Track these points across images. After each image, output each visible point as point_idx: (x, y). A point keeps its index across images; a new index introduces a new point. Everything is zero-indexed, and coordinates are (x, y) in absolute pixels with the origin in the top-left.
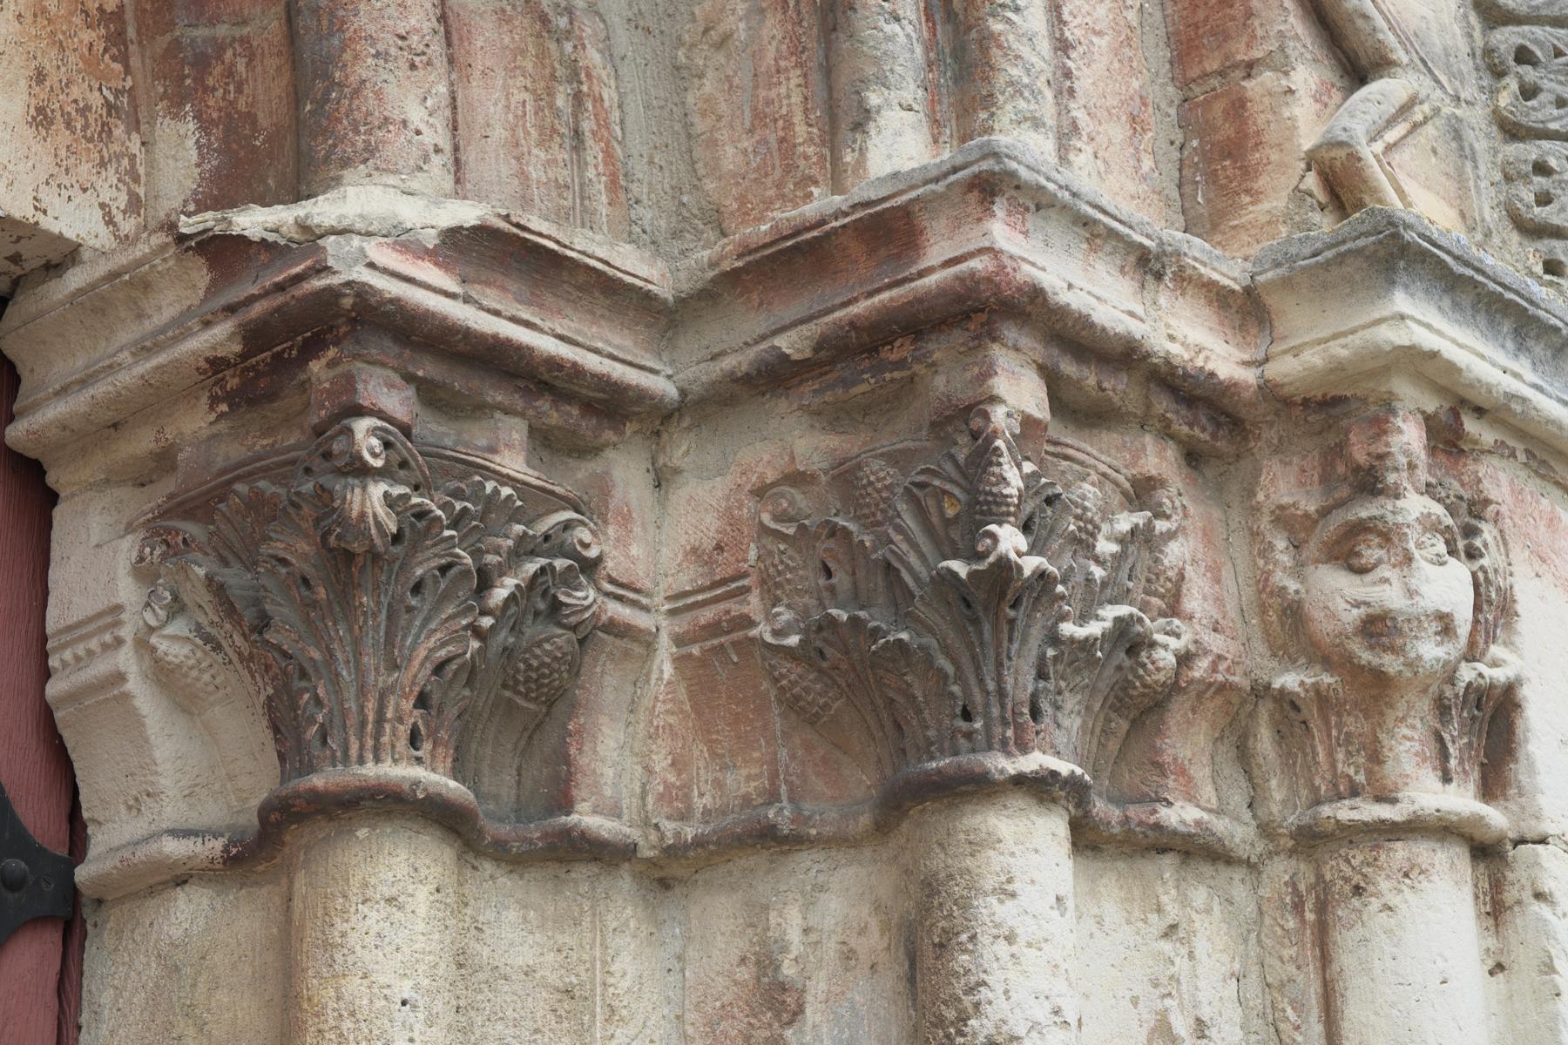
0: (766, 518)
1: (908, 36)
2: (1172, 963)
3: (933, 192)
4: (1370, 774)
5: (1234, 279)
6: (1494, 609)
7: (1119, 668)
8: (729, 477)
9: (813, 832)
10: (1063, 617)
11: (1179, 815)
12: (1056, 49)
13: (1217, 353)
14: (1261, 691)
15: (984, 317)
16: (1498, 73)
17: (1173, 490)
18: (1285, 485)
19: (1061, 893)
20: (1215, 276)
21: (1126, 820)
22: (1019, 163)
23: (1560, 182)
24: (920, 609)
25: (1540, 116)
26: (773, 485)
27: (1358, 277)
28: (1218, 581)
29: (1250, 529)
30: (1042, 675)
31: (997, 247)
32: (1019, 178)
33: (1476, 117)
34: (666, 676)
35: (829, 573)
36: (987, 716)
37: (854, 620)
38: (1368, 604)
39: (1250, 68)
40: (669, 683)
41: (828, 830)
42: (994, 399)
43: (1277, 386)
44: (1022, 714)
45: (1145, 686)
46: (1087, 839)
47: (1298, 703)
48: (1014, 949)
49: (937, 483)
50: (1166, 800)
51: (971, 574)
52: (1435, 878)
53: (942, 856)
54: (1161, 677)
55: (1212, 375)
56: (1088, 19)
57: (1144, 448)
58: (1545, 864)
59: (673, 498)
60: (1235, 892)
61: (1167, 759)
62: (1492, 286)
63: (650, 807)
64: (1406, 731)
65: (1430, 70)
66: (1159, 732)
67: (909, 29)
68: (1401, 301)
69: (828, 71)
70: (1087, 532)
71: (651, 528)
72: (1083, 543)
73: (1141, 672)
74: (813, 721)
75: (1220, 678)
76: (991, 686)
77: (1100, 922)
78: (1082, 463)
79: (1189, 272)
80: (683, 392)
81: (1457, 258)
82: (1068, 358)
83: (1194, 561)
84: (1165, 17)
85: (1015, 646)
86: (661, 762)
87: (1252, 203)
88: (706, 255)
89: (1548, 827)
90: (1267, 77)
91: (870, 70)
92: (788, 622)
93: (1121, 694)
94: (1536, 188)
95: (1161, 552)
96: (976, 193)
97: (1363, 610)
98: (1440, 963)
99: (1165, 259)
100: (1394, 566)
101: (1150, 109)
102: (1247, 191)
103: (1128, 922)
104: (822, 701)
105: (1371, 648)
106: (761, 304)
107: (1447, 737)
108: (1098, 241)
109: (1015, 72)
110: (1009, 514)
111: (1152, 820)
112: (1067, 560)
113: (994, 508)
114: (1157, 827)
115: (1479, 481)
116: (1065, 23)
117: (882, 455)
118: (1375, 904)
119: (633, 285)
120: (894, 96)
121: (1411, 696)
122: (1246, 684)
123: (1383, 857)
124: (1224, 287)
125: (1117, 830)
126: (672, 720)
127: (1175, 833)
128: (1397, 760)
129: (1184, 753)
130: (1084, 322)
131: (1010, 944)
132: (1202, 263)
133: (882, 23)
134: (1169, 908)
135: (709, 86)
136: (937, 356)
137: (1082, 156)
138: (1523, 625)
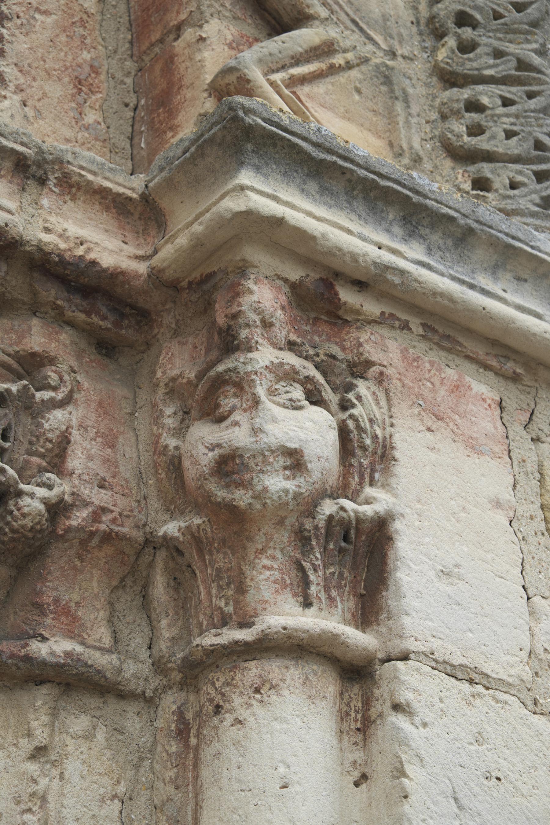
2: (35, 782)
4: (237, 603)
5: (133, 189)
6: (363, 455)
11: (54, 647)
13: (109, 248)
14: (151, 543)
16: (439, 35)
17: (64, 367)
18: (178, 361)
20: (107, 184)
23: (492, 116)
25: (475, 65)
27: (218, 166)
28: (112, 446)
33: (419, 69)
38: (219, 446)
45: (13, 531)
47: (181, 547)
50: (41, 635)
52: (286, 692)
54: (28, 522)
55: (94, 263)
57: (30, 328)
58: (402, 678)
60: (127, 724)
61: (46, 599)
62: (362, 173)
64: (266, 562)
65: (361, 30)
66: (42, 578)
68: (246, 177)
73: (9, 518)
75: (103, 527)
79: (75, 178)
81: (317, 145)
83: (82, 426)
87: (173, 137)
89: (412, 645)
90: (189, 34)
94: (469, 122)
95: (43, 417)
97: (217, 451)
98: (282, 770)
99: (46, 166)
100: (245, 411)
102: (171, 129)
105: (227, 486)
107: (307, 565)
111: (23, 652)
114: (27, 658)
115: (360, 345)
118: (229, 718)
121: (268, 528)
123: (238, 676)
124: (119, 195)
127: (44, 664)
128: (258, 588)
132: (90, 171)
138: (399, 469)
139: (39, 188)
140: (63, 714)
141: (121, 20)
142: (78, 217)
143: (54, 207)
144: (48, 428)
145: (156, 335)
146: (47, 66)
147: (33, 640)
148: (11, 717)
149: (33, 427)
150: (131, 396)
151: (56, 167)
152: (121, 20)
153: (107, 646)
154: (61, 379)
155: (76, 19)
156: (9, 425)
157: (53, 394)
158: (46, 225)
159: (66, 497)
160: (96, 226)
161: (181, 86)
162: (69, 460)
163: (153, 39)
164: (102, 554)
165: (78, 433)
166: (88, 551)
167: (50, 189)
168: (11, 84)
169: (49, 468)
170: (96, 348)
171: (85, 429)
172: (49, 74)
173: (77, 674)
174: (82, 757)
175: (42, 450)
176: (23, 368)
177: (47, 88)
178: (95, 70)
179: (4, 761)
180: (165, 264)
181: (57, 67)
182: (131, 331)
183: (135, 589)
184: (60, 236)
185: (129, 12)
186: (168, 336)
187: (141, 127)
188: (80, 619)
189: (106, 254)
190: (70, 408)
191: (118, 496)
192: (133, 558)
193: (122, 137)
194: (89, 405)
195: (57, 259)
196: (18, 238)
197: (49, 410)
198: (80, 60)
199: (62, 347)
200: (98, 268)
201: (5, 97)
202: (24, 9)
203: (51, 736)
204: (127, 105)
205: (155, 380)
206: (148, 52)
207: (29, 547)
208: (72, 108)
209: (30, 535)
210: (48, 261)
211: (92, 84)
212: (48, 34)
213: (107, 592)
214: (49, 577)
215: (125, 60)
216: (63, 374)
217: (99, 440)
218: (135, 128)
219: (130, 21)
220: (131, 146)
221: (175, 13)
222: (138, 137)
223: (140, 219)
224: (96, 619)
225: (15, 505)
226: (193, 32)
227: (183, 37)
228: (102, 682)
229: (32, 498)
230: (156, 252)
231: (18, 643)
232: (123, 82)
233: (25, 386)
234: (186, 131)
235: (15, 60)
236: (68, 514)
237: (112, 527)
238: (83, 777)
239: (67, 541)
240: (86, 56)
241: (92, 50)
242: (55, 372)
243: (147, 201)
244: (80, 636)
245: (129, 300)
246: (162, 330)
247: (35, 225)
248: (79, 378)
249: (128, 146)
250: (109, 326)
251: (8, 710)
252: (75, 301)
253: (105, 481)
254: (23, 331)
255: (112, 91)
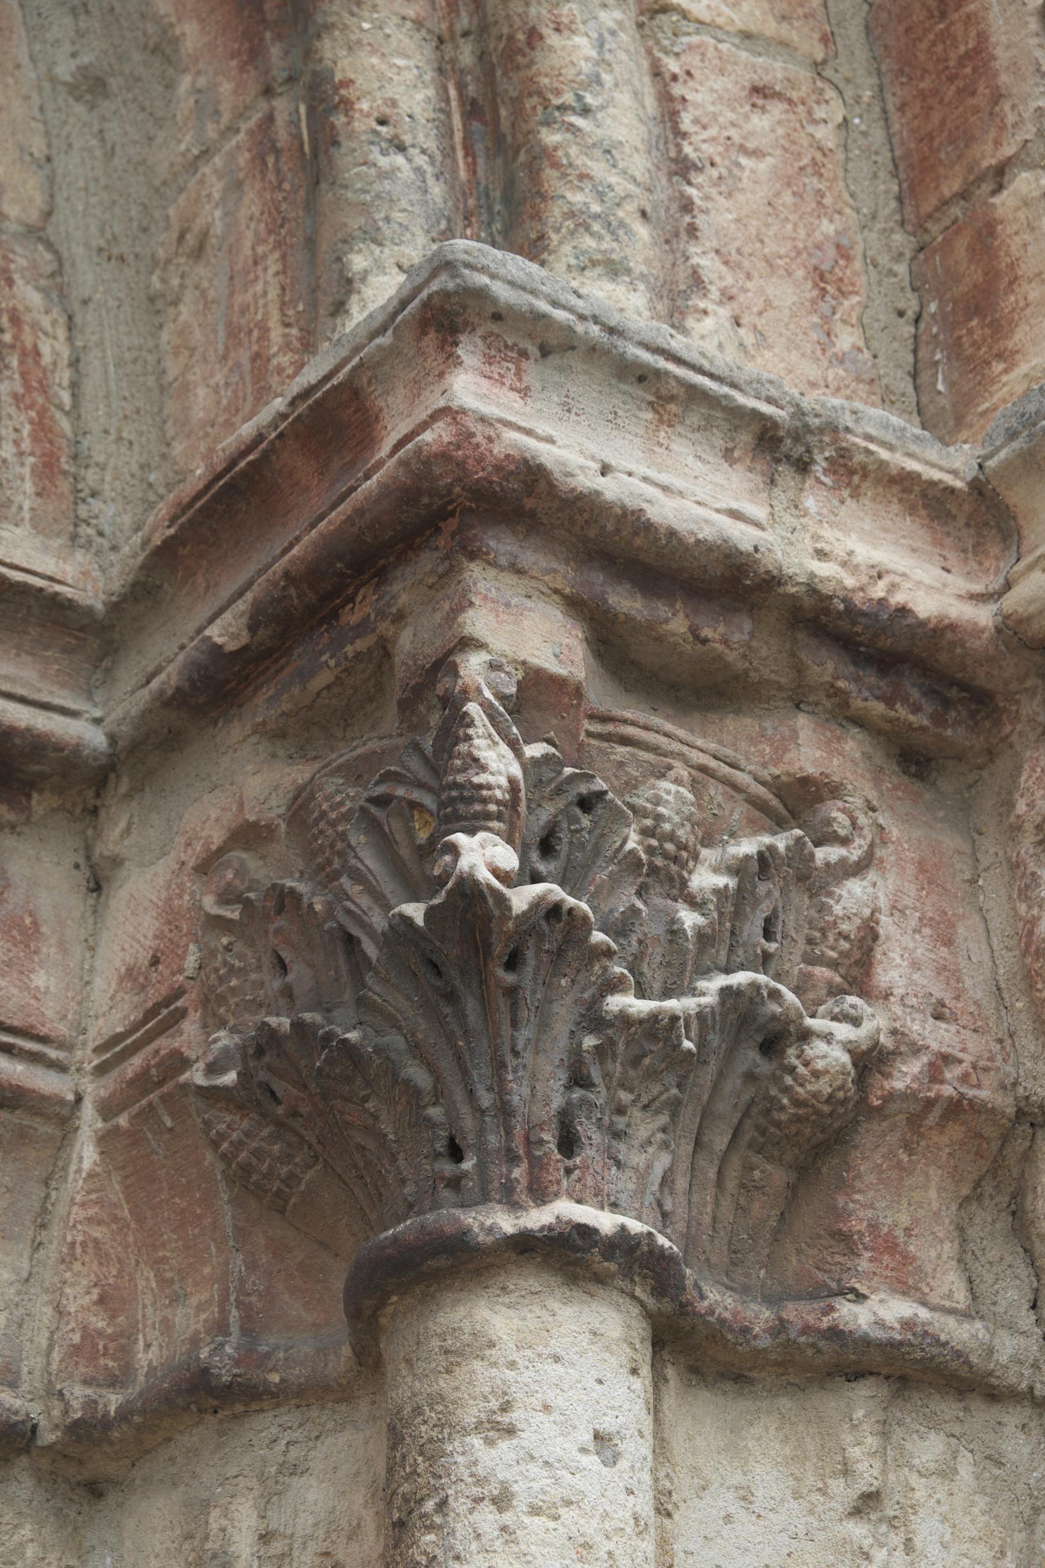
0: (209, 904)
1: (418, 170)
3: (380, 348)
5: (955, 473)
7: (750, 1077)
8: (173, 854)
9: (275, 1378)
10: (614, 986)
11: (878, 1312)
12: (671, 174)
13: (926, 584)
15: (453, 523)
17: (856, 802)
19: (608, 1424)
21: (781, 1326)
22: (493, 276)
24: (376, 989)
26: (221, 851)
28: (948, 943)
29: (1009, 860)
30: (578, 1079)
31: (455, 405)
32: (494, 300)
34: (86, 1165)
35: (283, 967)
36: (481, 1149)
37: (298, 1026)
39: (1000, 174)
40: (91, 1175)
41: (297, 1374)
42: (468, 643)
43: (1020, 621)
44: (541, 1142)
45: (797, 1103)
46: (685, 1349)
48: (508, 1518)
49: (400, 792)
50: (853, 1290)
51: (429, 914)
53: (409, 1379)
54: (823, 1086)
55: (903, 611)
56: (732, 132)
57: (795, 734)
59: (113, 903)
60: (1007, 1447)
63: (54, 1367)
66: (844, 1186)
67: (422, 161)
69: (311, 243)
70: (666, 856)
71: (77, 951)
72: (663, 871)
73: (789, 1080)
74: (279, 1204)
75: (947, 1091)
76: (486, 1100)
77: (746, 1497)
78: (654, 749)
79: (859, 458)
80: (113, 739)
82: (624, 589)
83: (895, 908)
84: (890, 137)
85: (525, 1034)
86: (79, 1298)
87: (1006, 371)
88: (127, 520)
91: (356, 223)
92: (226, 1050)
93: (762, 1121)
95: (830, 894)
96: (432, 335)
99: (809, 438)
101: (858, 264)
102: (1000, 356)
103: (797, 1495)
104: (284, 1170)
106: (207, 588)
108: (673, 408)
109: (577, 198)
110: (488, 816)
111: (826, 1322)
112: (626, 898)
113: (461, 808)
114: (835, 1333)
116: (684, 135)
117: (339, 769)
119: (25, 585)
120: (388, 254)
122: (1006, 1104)
124: (933, 484)
125: (765, 1342)
126: (97, 1232)
127: (866, 1342)
129: (896, 1217)
130: (633, 521)
131: (501, 1510)
132: (883, 444)
133: (375, 155)
134: (862, 1467)
135: (186, 312)
136: (403, 599)
137: (709, 322)
139: (798, 478)
140: (898, 1433)
141: (879, 159)
142: (866, 527)
143: (825, 511)
144: (841, 913)
145: (1007, 736)
146: (766, 250)
147: (839, 1299)
148: (808, 1440)
149: (813, 912)
150: (967, 848)
151: (827, 439)
152: (879, 159)
153: (961, 1306)
154: (854, 824)
155: (805, 161)
156: (775, 911)
157: (843, 851)
158: (818, 546)
159: (883, 1039)
160: (896, 543)
161: (1016, 278)
162: (879, 970)
163: (947, 193)
164: (944, 1140)
165: (890, 920)
166: (921, 1135)
167: (817, 479)
168: (713, 288)
169: (846, 987)
170: (899, 764)
171: (902, 912)
172: (771, 266)
173: (923, 1358)
174: (939, 1510)
175: (833, 954)
176: (785, 806)
177: (770, 291)
178: (844, 253)
179: (803, 1520)
180: (1031, 609)
181: (783, 251)
182: (961, 731)
183: (997, 1200)
184: (844, 564)
185: (891, 143)
186: (1032, 737)
187: (933, 353)
188: (914, 1258)
189: (921, 593)
190: (872, 875)
191: (967, 1034)
192: (995, 1146)
193: (899, 373)
194: (904, 869)
195: (842, 607)
196: (775, 572)
197: (839, 880)
198: (818, 236)
199: (849, 764)
200: (910, 620)
201: (705, 312)
202: (720, 149)
203: (884, 1472)
204: (901, 314)
205: (1012, 819)
206: (938, 215)
207: (823, 1131)
208: (815, 326)
209: (826, 1109)
210: (826, 611)
211: (841, 280)
212: (763, 192)
213: (954, 1207)
214: (858, 1184)
215: (892, 230)
216: (857, 814)
217: (926, 931)
218: (920, 354)
219: (893, 160)
220: (916, 388)
221: (990, 143)
222: (930, 372)
223: (967, 525)
224: (939, 1257)
225: (798, 1057)
226: (1032, 179)
227: (1011, 188)
228: (964, 1372)
229: (829, 1043)
230: (1008, 586)
231: (815, 1306)
232: (892, 273)
233: (799, 840)
234: (1034, 362)
235: (715, 244)
236: (887, 1069)
237: (962, 1090)
238: (945, 1546)
239: (886, 1118)
240: (828, 227)
241: (836, 216)
242: (843, 811)
243: (980, 493)
244: (918, 1289)
245: (959, 675)
246: (1019, 727)
247: (799, 546)
248: (881, 821)
249: (910, 389)
250: (926, 722)
251: (801, 1428)
252: (867, 680)
253: (944, 1006)
254: (783, 738)
255: (874, 287)
